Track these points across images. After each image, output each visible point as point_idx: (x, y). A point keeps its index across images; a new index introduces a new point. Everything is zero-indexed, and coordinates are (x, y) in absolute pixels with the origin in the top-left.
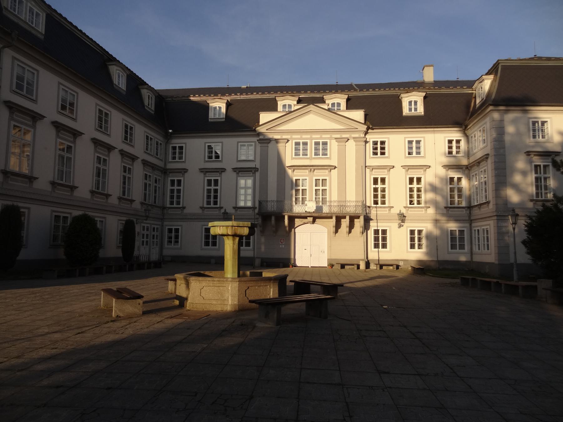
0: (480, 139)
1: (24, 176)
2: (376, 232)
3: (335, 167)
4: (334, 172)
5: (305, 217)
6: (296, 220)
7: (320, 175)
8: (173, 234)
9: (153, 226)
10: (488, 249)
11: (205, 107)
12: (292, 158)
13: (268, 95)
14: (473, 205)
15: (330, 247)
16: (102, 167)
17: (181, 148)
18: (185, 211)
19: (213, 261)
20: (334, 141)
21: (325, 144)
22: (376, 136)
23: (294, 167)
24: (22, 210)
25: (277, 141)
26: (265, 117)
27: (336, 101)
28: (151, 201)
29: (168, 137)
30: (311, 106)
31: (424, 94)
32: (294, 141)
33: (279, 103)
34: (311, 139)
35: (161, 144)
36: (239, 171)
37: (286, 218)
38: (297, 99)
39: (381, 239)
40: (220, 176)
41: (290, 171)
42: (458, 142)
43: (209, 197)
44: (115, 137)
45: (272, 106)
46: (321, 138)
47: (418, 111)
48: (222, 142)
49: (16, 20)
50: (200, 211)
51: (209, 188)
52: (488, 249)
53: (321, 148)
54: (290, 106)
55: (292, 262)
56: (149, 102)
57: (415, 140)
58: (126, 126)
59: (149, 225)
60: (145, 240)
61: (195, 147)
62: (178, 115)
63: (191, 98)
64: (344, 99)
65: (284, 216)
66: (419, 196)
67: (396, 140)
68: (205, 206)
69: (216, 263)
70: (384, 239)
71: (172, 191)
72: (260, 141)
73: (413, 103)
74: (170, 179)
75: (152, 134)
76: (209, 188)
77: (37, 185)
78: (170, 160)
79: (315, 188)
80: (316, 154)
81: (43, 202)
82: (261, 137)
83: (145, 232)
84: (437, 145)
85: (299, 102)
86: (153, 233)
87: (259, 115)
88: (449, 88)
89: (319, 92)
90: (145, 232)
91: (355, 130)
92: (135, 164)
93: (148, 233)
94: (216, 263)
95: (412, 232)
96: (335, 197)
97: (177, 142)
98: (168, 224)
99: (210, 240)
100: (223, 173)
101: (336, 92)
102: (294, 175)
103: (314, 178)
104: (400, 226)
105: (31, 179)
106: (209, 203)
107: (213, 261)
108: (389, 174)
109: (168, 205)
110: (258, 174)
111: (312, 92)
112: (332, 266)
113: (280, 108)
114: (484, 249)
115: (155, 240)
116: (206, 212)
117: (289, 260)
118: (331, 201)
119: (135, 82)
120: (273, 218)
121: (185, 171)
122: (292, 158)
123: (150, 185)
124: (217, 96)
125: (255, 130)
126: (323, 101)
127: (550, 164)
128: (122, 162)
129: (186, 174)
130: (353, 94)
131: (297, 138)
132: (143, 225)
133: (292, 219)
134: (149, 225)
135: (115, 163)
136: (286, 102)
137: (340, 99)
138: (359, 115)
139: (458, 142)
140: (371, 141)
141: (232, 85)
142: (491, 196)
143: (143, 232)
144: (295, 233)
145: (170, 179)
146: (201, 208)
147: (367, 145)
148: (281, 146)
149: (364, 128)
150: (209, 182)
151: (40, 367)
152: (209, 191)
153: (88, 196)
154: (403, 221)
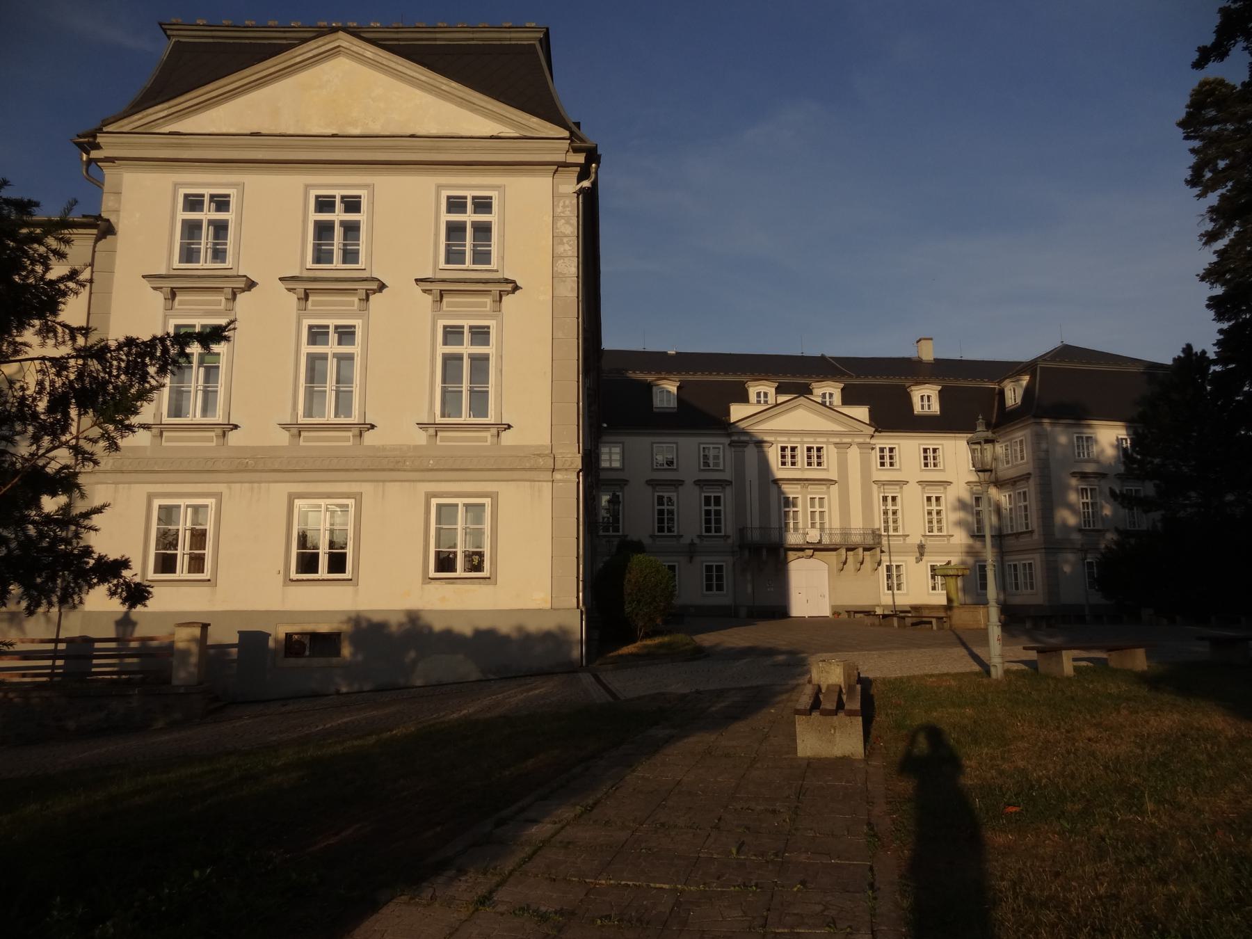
0: (1011, 452)
2: (889, 568)
4: (834, 489)
5: (802, 550)
7: (816, 491)
14: (1005, 532)
15: (832, 589)
20: (832, 447)
22: (885, 441)
26: (737, 412)
27: (828, 390)
31: (939, 388)
34: (802, 443)
39: (893, 578)
43: (708, 521)
47: (933, 409)
48: (623, 443)
52: (1032, 588)
53: (815, 455)
57: (887, 447)
66: (939, 521)
67: (909, 447)
70: (709, 578)
73: (926, 399)
79: (810, 510)
82: (735, 438)
84: (956, 453)
88: (805, 391)
91: (859, 433)
95: (709, 568)
96: (836, 524)
102: (790, 491)
104: (919, 560)
106: (708, 530)
108: (901, 492)
113: (753, 397)
118: (830, 529)
120: (764, 552)
136: (762, 389)
138: (862, 413)
140: (878, 447)
142: (1034, 523)
150: (707, 500)
152: (708, 513)
154: (922, 555)
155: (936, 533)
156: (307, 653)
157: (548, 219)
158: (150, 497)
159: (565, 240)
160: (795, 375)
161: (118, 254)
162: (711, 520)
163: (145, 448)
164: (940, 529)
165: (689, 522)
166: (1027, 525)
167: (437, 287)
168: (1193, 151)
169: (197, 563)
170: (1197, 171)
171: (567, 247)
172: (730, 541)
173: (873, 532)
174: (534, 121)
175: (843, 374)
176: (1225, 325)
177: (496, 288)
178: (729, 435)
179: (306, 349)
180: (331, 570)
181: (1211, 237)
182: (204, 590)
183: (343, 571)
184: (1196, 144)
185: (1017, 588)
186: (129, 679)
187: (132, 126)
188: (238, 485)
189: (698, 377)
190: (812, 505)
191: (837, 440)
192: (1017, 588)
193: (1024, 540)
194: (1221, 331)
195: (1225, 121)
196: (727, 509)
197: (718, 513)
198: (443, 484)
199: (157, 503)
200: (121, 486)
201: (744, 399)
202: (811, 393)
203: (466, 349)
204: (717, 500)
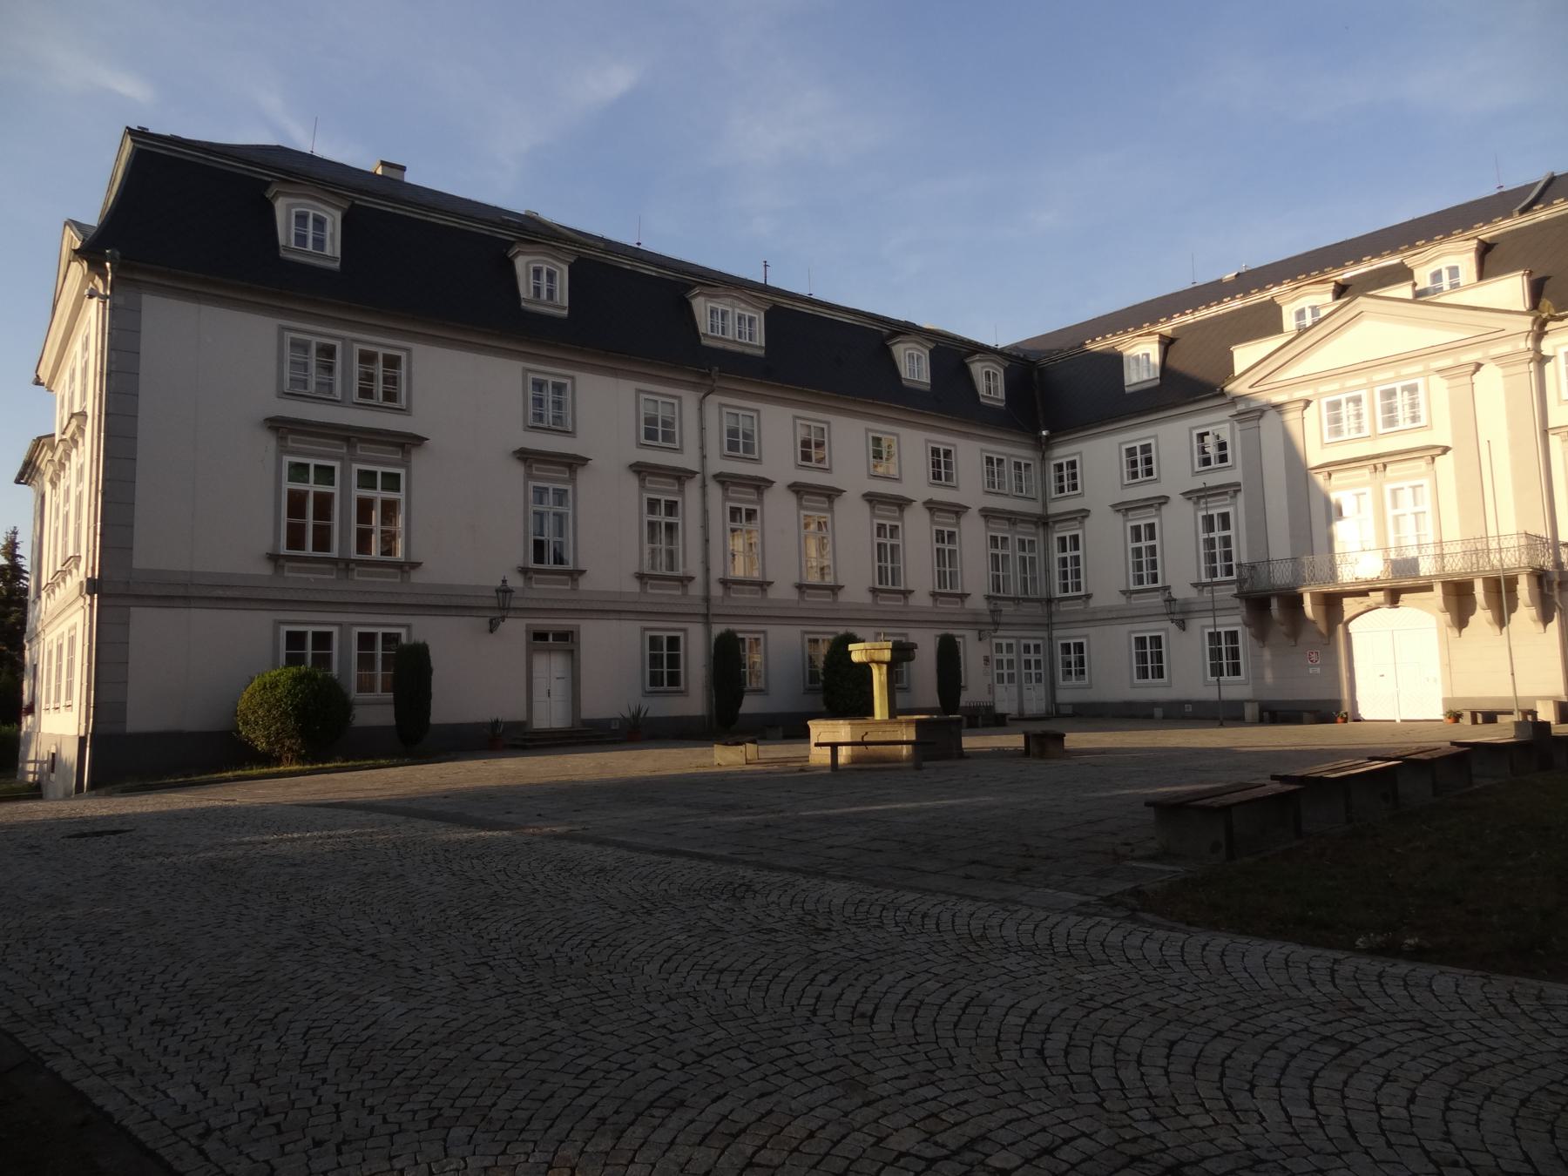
1: (752, 583)
3: (1446, 450)
5: (1364, 593)
6: (1346, 601)
8: (1073, 657)
9: (1023, 642)
11: (1115, 361)
12: (1324, 445)
13: (1258, 296)
15: (1448, 665)
16: (888, 541)
17: (1073, 464)
18: (1093, 603)
19: (1158, 712)
23: (1331, 467)
24: (740, 636)
25: (1278, 408)
26: (1245, 356)
27: (1443, 264)
28: (1014, 589)
29: (1043, 447)
30: (1361, 299)
32: (1324, 401)
33: (1285, 309)
34: (1371, 385)
35: (1027, 466)
36: (1199, 498)
37: (1307, 599)
38: (1331, 286)
40: (1159, 516)
41: (1320, 478)
43: (1211, 558)
44: (916, 483)
45: (1265, 321)
46: (1398, 378)
49: (719, 345)
50: (1122, 600)
51: (1138, 545)
54: (1315, 309)
55: (1346, 708)
56: (989, 383)
58: (935, 452)
59: (1013, 641)
60: (1005, 671)
61: (1099, 456)
62: (1055, 392)
63: (1089, 347)
64: (1467, 251)
65: (1300, 598)
68: (1132, 587)
69: (1164, 717)
70: (1142, 658)
71: (1064, 562)
72: (1241, 417)
74: (1056, 535)
75: (997, 450)
76: (1138, 545)
77: (773, 594)
78: (1054, 495)
81: (784, 617)
82: (1241, 407)
83: (1005, 656)
85: (1341, 290)
86: (1025, 656)
87: (1231, 353)
89: (1394, 250)
90: (1005, 656)
91: (1499, 336)
92: (964, 521)
93: (1013, 656)
94: (1164, 717)
97: (1063, 453)
98: (1063, 635)
100: (1164, 508)
101: (1448, 234)
105: (763, 585)
107: (1158, 712)
109: (1058, 595)
110: (1241, 497)
111: (1377, 254)
112: (1456, 717)
113: (1289, 323)
115: (1033, 671)
116: (1137, 601)
117: (1337, 703)
119: (952, 355)
121: (1083, 514)
122: (1324, 445)
123: (1005, 557)
124: (1141, 327)
125: (1222, 394)
126: (1403, 274)
127: (354, 694)
128: (933, 522)
129: (1087, 521)
130: (1487, 232)
131: (1330, 390)
132: (995, 641)
133: (1332, 603)
134: (1013, 641)
135: (917, 531)
136: (1303, 301)
137: (1458, 255)
138: (1511, 289)
141: (1203, 279)
143: (999, 656)
144: (1348, 636)
145: (1056, 535)
146: (1195, 585)
147: (1549, 367)
148: (1292, 419)
149: (1526, 323)
150: (1209, 520)
152: (1210, 543)
153: (867, 598)
160: (1362, 264)
162: (1217, 554)
165: (1182, 564)
175: (1468, 227)
183: (289, 634)
189: (1189, 319)
191: (1447, 362)
196: (1238, 533)
197: (1226, 541)
204: (1225, 518)
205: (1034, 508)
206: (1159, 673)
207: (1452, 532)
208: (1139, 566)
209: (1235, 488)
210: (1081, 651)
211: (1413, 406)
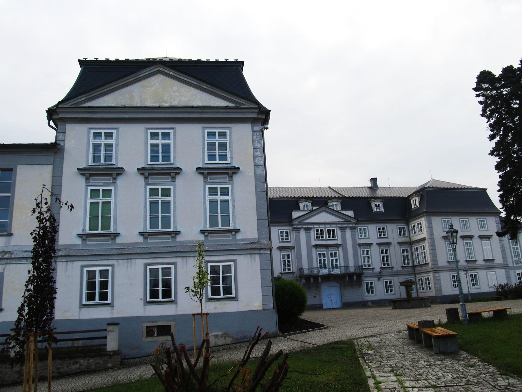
4: (340, 249)
10: (430, 289)
12: (315, 240)
19: (370, 304)
20: (338, 229)
21: (333, 230)
34: (325, 228)
40: (370, 249)
42: (404, 228)
51: (154, 199)
52: (430, 289)
53: (332, 234)
70: (372, 288)
76: (154, 199)
80: (329, 237)
82: (295, 227)
91: (348, 222)
99: (160, 288)
103: (330, 252)
114: (427, 289)
139: (404, 228)
151: (246, 357)
152: (383, 257)
155: (386, 266)
156: (156, 335)
157: (251, 141)
158: (83, 267)
159: (258, 150)
161: (64, 159)
163: (79, 245)
164: (388, 265)
166: (426, 260)
167: (205, 172)
168: (481, 103)
169: (104, 296)
170: (484, 111)
171: (259, 153)
172: (295, 275)
173: (359, 266)
174: (242, 101)
176: (501, 173)
177: (231, 171)
178: (292, 225)
179: (149, 199)
180: (101, 299)
181: (492, 137)
182: (108, 309)
184: (481, 99)
185: (423, 289)
186: (500, 314)
187: (70, 104)
188: (122, 261)
190: (320, 257)
192: (423, 289)
193: (425, 268)
194: (500, 177)
195: (491, 90)
196: (293, 259)
198: (212, 257)
199: (86, 269)
200: (69, 262)
201: (298, 209)
202: (328, 205)
203: (219, 198)
205: (407, 240)
206: (372, 292)
207: (351, 263)
208: (383, 261)
209: (337, 246)
210: (429, 280)
211: (365, 233)
